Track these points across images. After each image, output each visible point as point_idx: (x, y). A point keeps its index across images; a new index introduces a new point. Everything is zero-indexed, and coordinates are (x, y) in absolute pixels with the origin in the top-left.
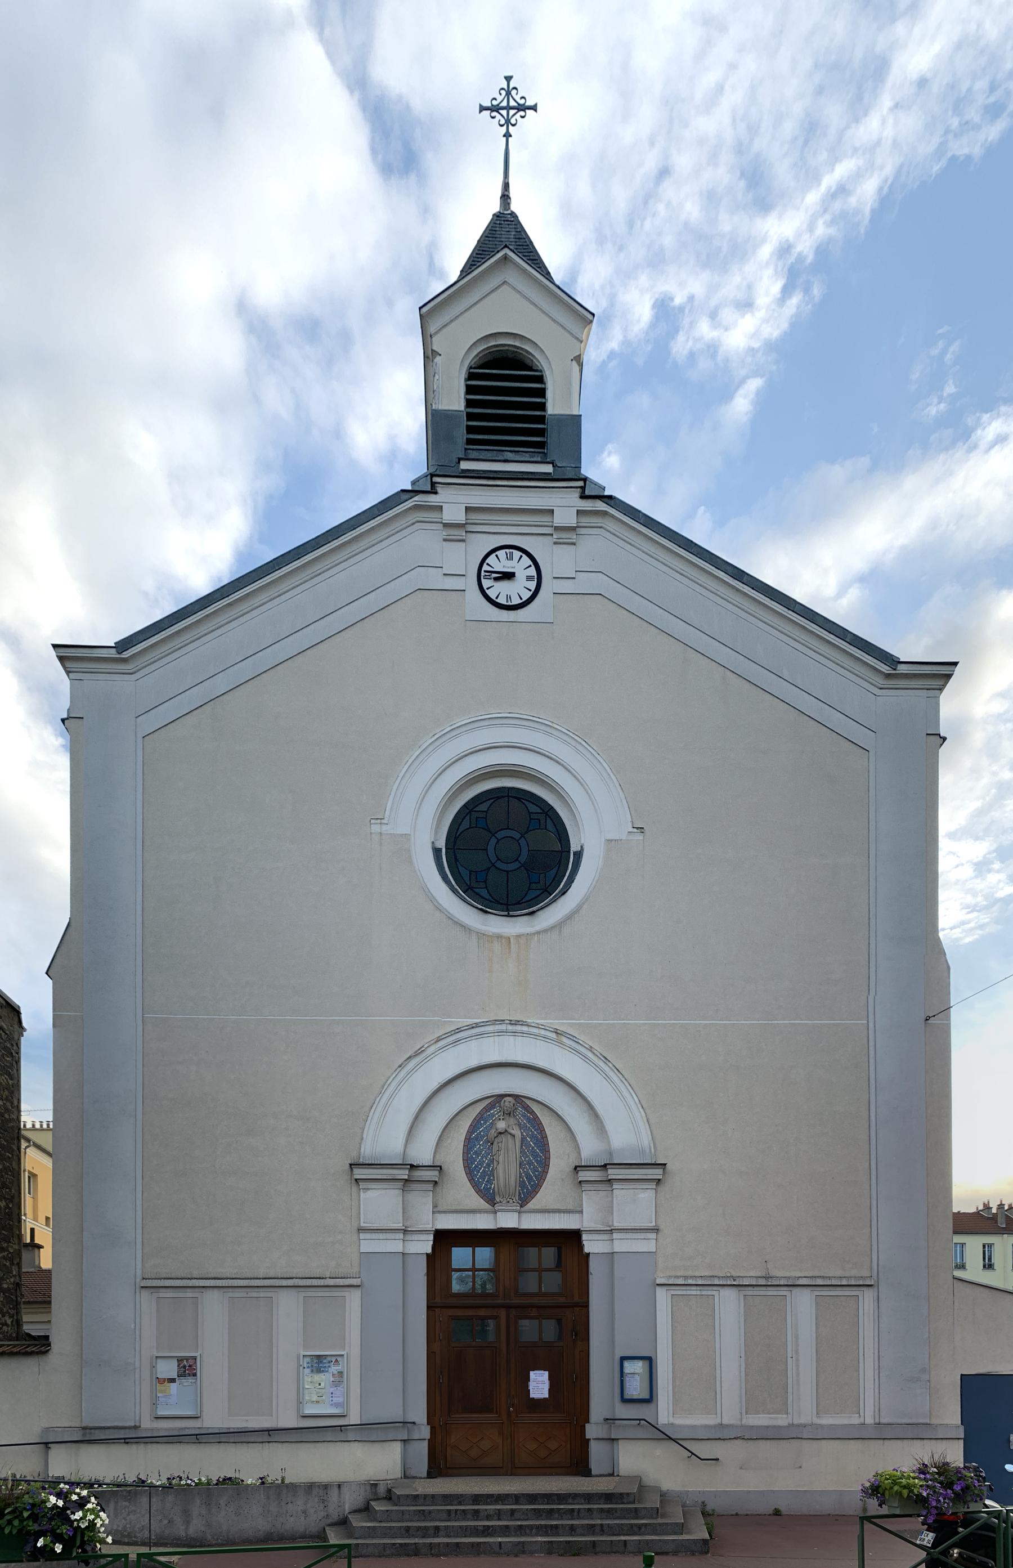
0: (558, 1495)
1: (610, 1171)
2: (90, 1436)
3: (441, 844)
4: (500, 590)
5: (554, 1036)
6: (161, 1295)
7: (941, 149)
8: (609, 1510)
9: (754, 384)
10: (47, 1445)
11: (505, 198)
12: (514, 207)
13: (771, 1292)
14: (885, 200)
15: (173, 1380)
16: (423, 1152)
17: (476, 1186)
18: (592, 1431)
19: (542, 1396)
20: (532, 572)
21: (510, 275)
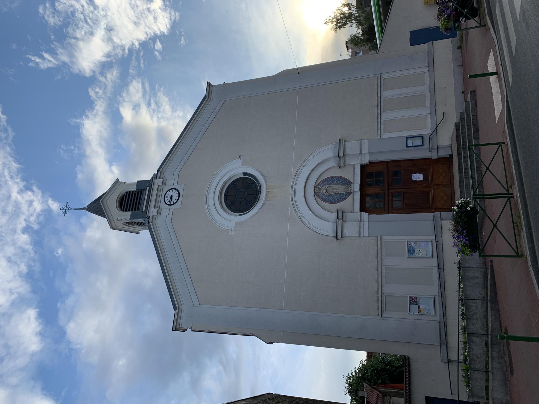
2: (444, 342)
3: (238, 214)
4: (174, 199)
7: (10, 145)
8: (462, 127)
9: (50, 202)
11: (83, 209)
13: (382, 104)
14: (17, 161)
15: (419, 307)
16: (333, 216)
17: (344, 199)
20: (171, 191)
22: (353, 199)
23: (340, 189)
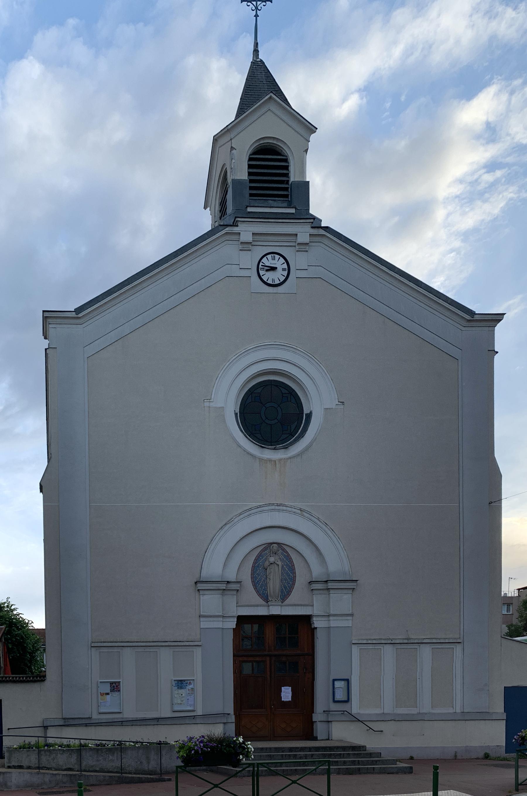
0: (330, 747)
1: (329, 584)
2: (68, 722)
3: (238, 411)
4: (268, 276)
5: (299, 512)
6: (101, 651)
8: (358, 754)
10: (46, 728)
11: (256, 51)
12: (261, 57)
15: (108, 694)
16: (231, 576)
18: (316, 717)
19: (288, 700)
20: (285, 266)
21: (272, 106)
22: (257, 606)
23: (274, 584)
